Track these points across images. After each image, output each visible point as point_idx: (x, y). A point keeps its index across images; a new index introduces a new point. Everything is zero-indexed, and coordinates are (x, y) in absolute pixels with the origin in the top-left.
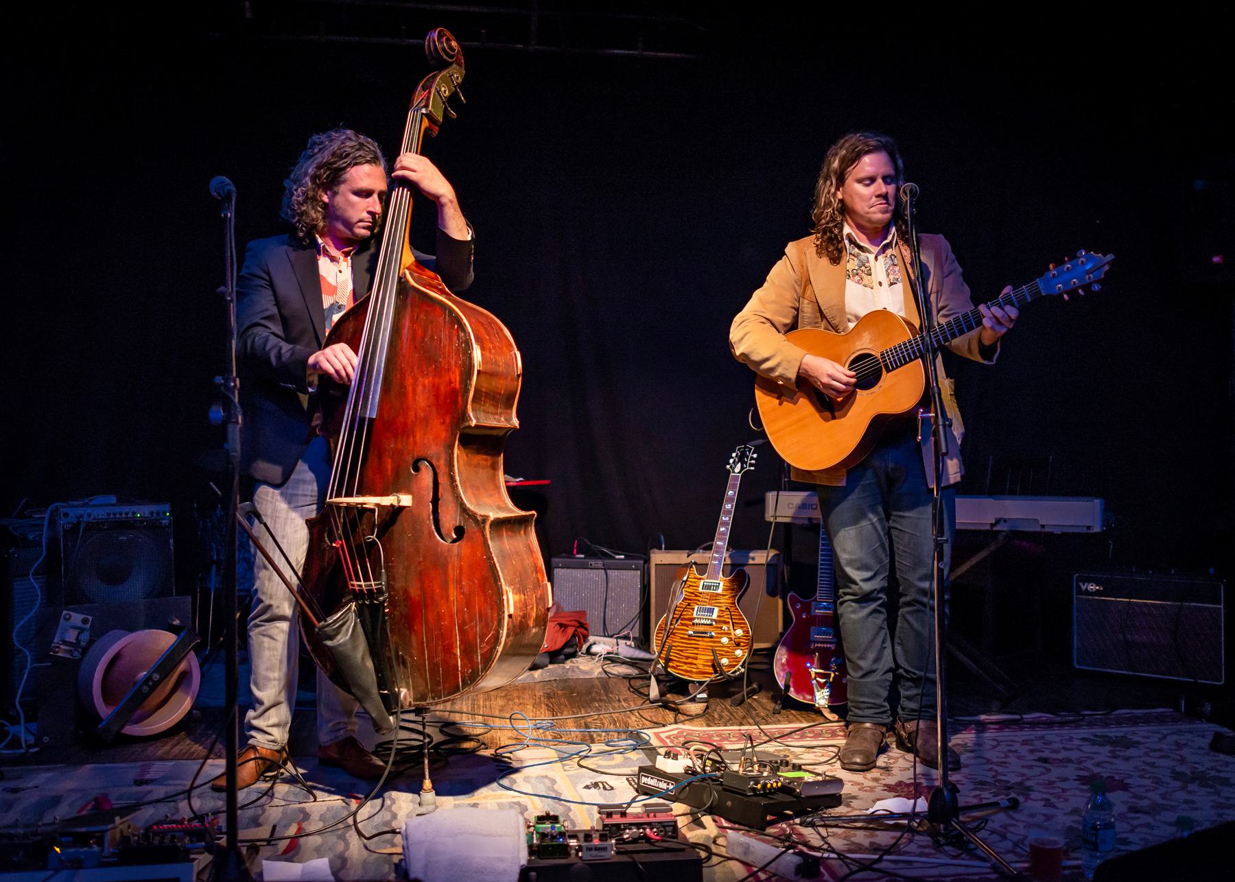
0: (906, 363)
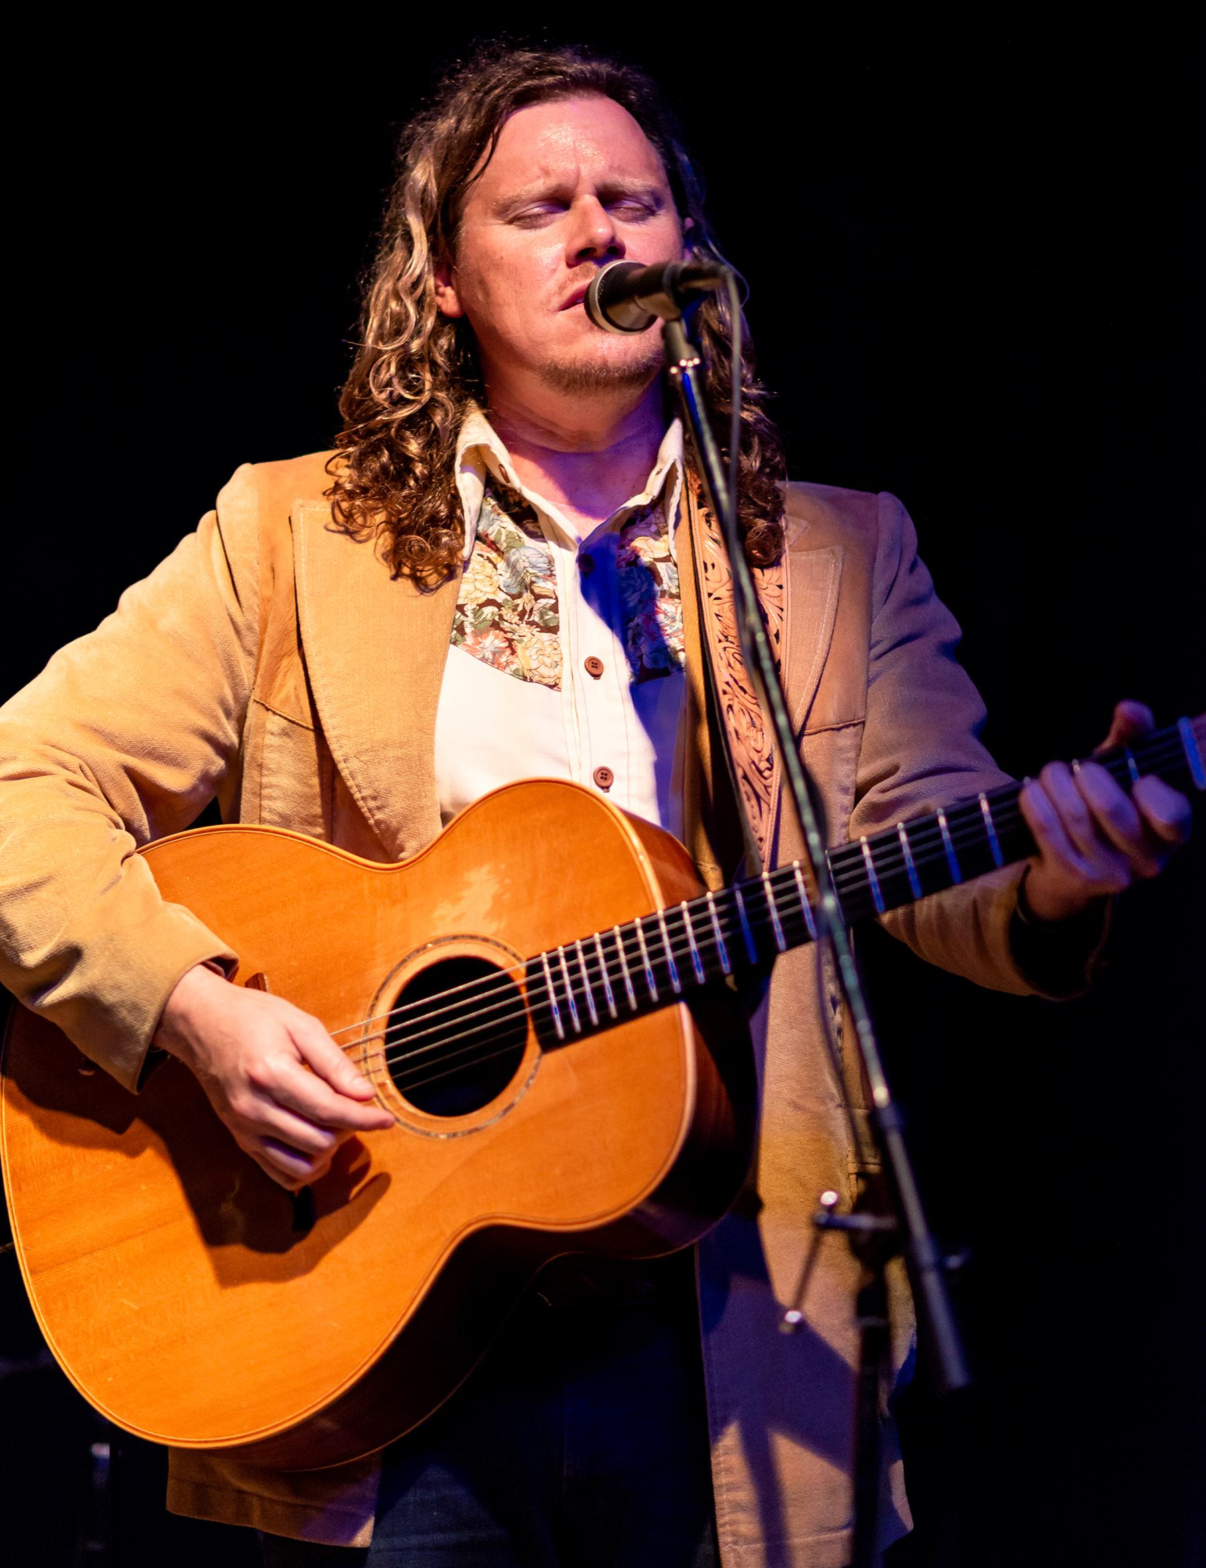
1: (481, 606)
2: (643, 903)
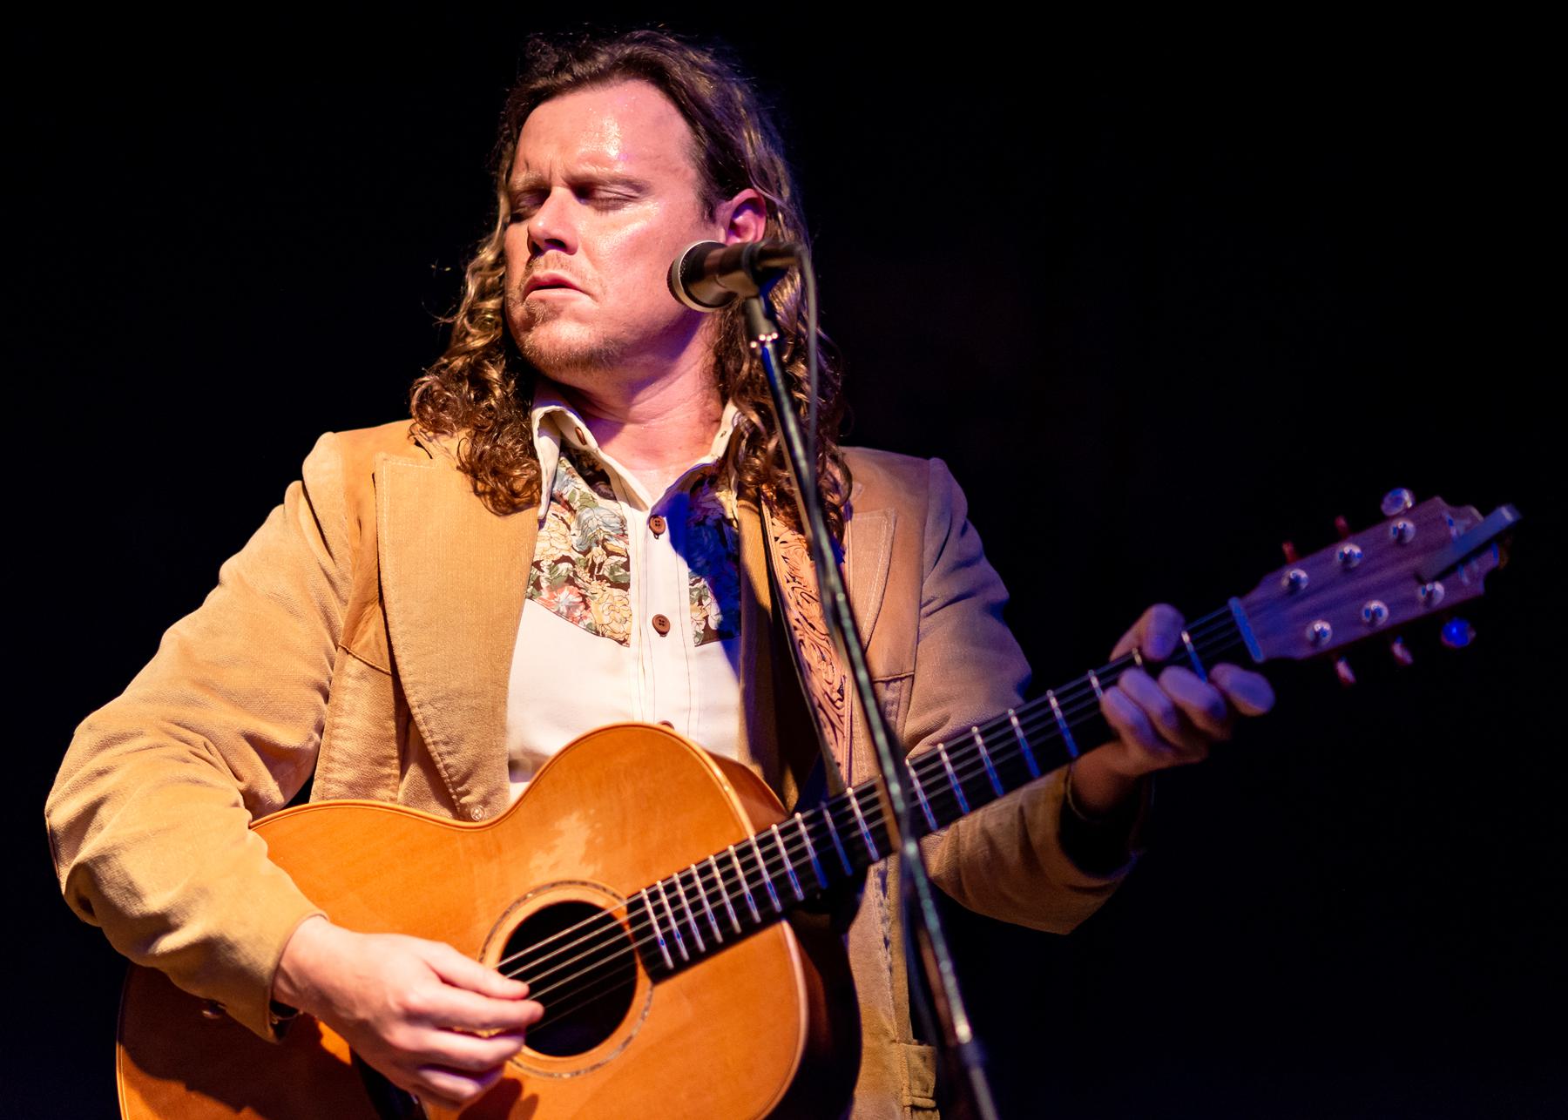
0: (731, 939)
1: (557, 562)
2: (735, 830)
